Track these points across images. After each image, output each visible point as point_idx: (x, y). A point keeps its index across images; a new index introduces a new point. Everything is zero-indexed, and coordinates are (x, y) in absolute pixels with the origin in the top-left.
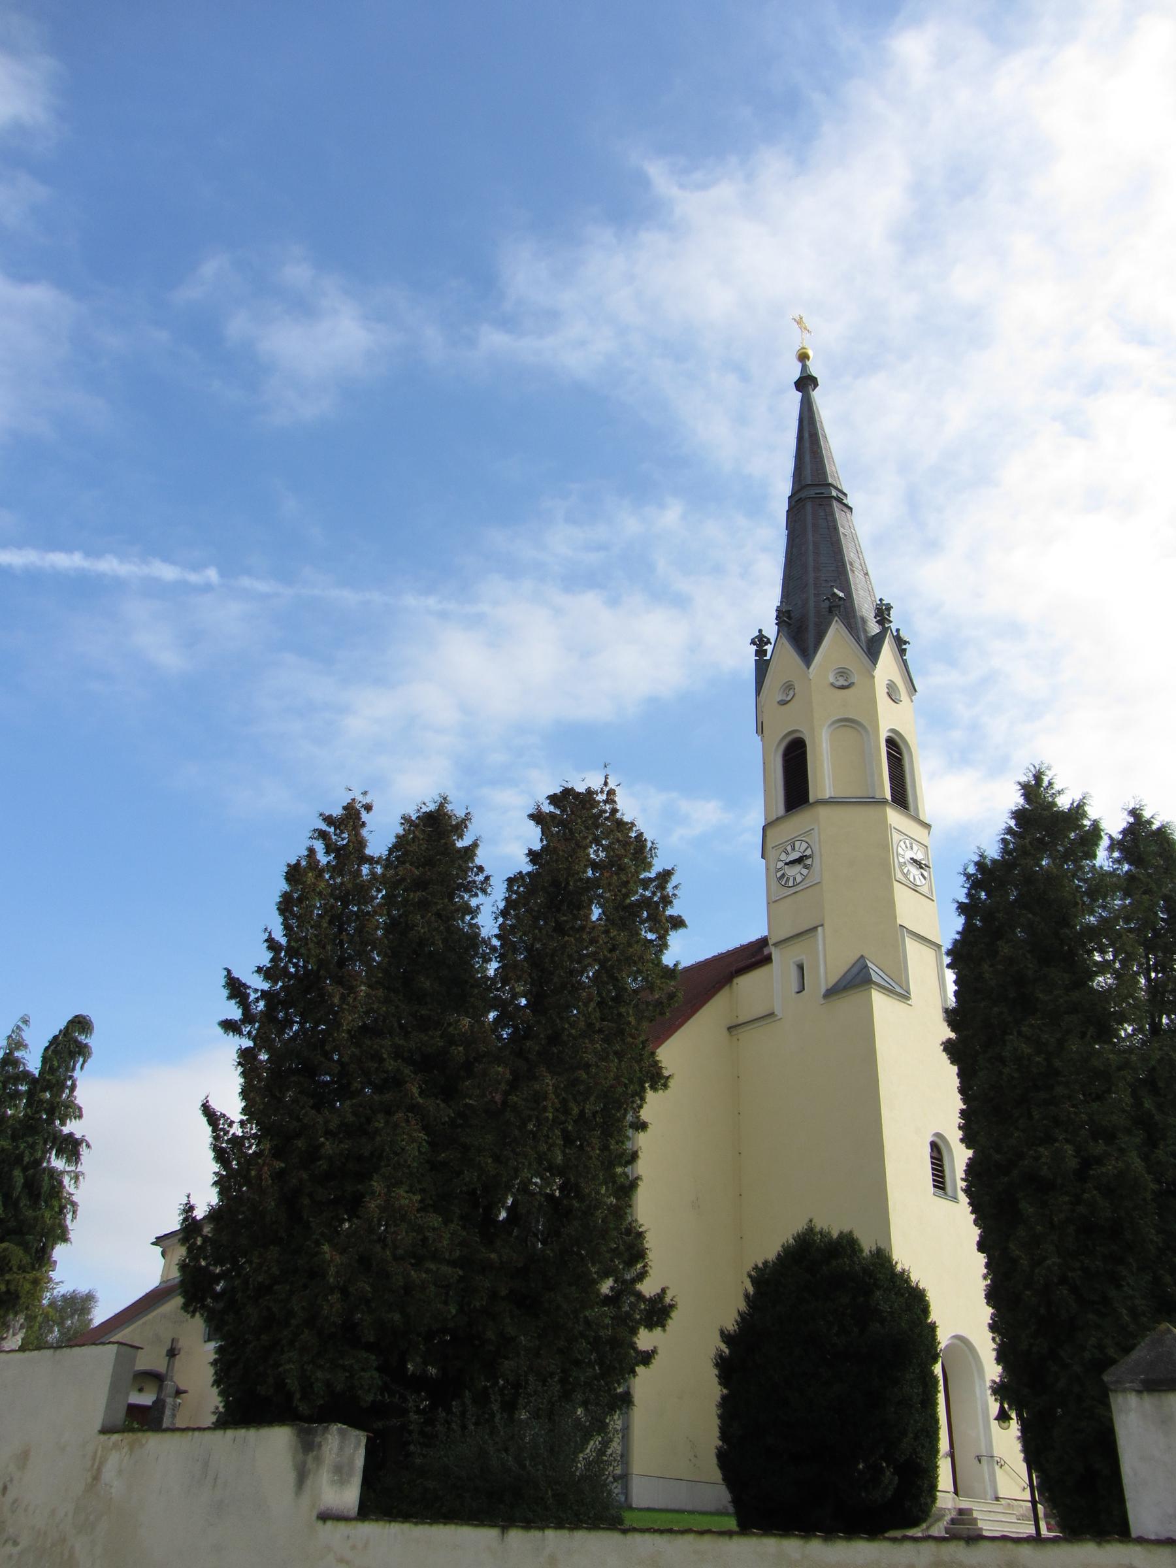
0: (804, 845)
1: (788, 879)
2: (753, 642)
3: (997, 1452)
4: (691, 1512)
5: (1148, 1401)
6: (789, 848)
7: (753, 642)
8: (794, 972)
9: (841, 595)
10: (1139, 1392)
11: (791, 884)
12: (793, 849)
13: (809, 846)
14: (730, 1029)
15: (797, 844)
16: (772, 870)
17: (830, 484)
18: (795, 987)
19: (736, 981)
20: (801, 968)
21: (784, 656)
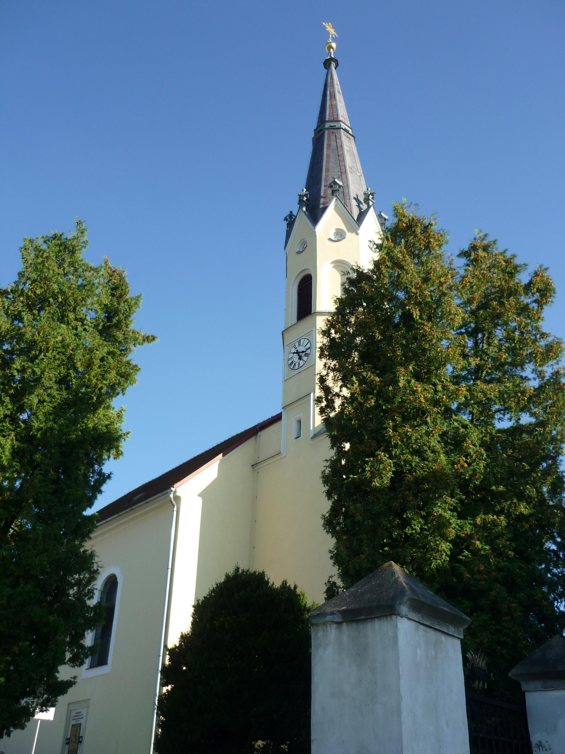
0: (306, 341)
1: (295, 364)
2: (286, 219)
3: (341, 118)
4: (452, 636)
5: (347, 630)
6: (297, 345)
7: (286, 219)
8: (295, 425)
9: (341, 184)
10: (339, 623)
11: (296, 367)
12: (299, 345)
13: (309, 342)
14: (252, 466)
15: (302, 341)
16: (286, 360)
17: (340, 121)
18: (295, 435)
19: (259, 434)
20: (299, 422)
21: (302, 220)
